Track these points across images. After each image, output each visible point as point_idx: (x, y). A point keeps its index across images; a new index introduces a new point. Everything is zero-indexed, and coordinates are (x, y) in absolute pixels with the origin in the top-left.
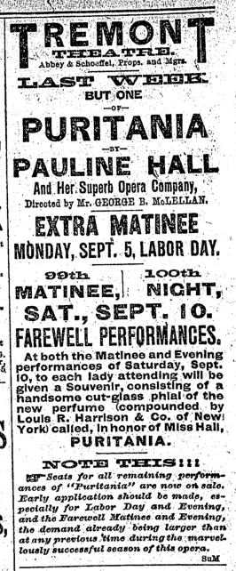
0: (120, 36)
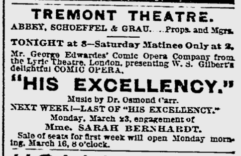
0: (79, 15)
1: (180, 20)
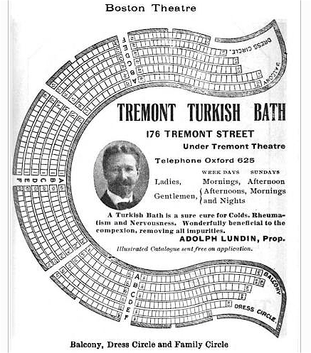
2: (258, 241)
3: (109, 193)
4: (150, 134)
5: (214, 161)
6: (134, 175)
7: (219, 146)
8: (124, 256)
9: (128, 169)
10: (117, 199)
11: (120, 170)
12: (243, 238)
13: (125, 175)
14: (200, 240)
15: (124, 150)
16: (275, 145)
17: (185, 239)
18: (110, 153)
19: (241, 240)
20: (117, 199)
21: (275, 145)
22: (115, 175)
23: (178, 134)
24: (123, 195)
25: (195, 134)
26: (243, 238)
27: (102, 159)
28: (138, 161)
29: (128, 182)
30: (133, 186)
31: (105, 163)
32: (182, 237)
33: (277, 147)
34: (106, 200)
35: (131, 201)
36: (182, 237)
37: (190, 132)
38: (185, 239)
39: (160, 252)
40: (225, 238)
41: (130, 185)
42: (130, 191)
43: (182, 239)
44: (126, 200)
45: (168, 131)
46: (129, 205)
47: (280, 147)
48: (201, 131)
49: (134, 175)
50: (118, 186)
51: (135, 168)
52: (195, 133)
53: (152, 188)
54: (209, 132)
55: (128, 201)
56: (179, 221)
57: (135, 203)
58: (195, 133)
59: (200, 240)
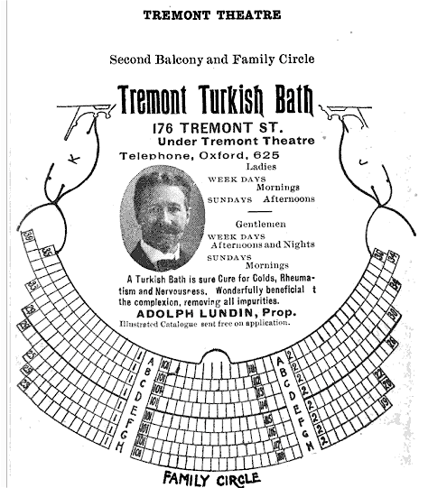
1: (364, 124)
2: (256, 316)
3: (144, 246)
4: (158, 128)
5: (226, 179)
6: (182, 218)
7: (212, 141)
8: (125, 331)
9: (173, 208)
10: (156, 256)
11: (160, 208)
12: (233, 313)
13: (168, 218)
14: (168, 316)
15: (166, 180)
16: (299, 139)
17: (145, 314)
18: (145, 184)
19: (231, 316)
20: (156, 256)
21: (299, 139)
22: (152, 218)
23: (199, 128)
24: (164, 250)
25: (227, 128)
26: (233, 313)
27: (133, 195)
28: (187, 195)
29: (173, 229)
30: (180, 235)
31: (138, 201)
32: (141, 311)
33: (301, 141)
34: (139, 256)
35: (178, 257)
36: (141, 311)
37: (218, 124)
38: (145, 314)
39: (135, 328)
40: (206, 313)
41: (175, 232)
42: (175, 244)
43: (140, 314)
44: (169, 256)
45: (185, 124)
46: (174, 265)
47: (306, 142)
48: (235, 124)
49: (182, 218)
50: (157, 234)
51: (183, 207)
52: (227, 127)
53: (206, 243)
54: (248, 124)
55: (172, 258)
56: (210, 289)
57: (184, 259)
58: (227, 127)
59: (168, 316)
